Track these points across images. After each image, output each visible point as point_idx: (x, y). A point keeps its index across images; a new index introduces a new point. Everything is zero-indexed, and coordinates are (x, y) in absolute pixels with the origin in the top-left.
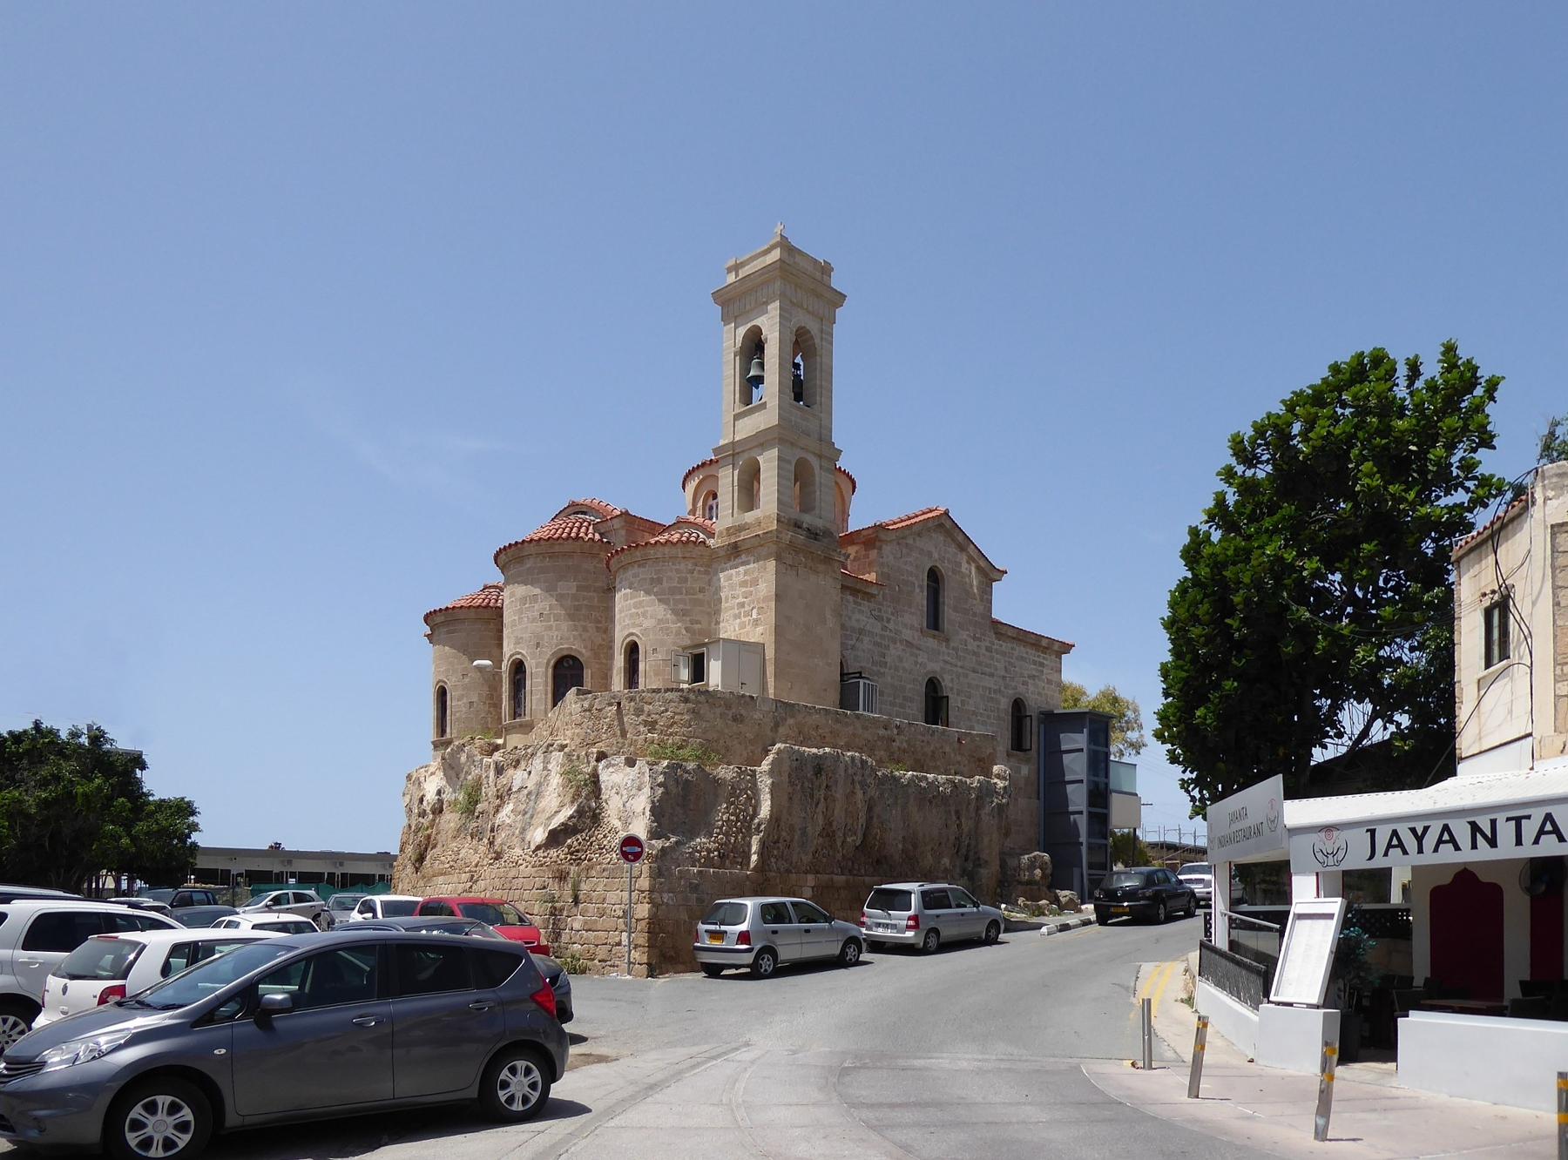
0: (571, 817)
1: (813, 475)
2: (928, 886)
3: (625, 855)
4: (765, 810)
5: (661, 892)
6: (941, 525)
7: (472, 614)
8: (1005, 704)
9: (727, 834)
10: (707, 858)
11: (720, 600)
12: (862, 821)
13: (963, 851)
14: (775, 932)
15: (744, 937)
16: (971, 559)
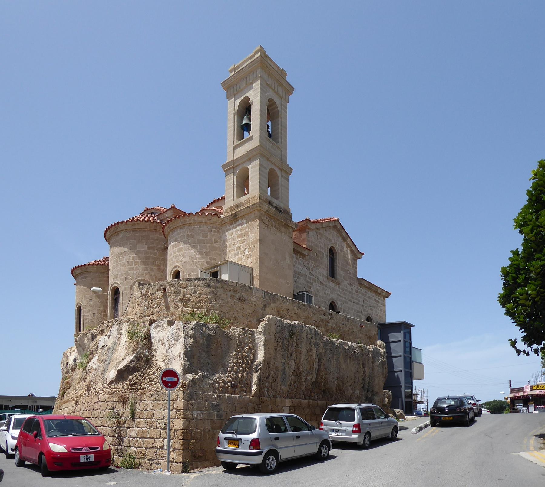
0: (132, 361)
1: (278, 181)
2: (363, 406)
3: (165, 383)
4: (261, 356)
5: (192, 411)
6: (335, 227)
7: (95, 268)
9: (236, 372)
10: (224, 387)
11: (226, 247)
12: (316, 367)
13: (366, 387)
14: (277, 439)
15: (255, 443)
16: (348, 246)
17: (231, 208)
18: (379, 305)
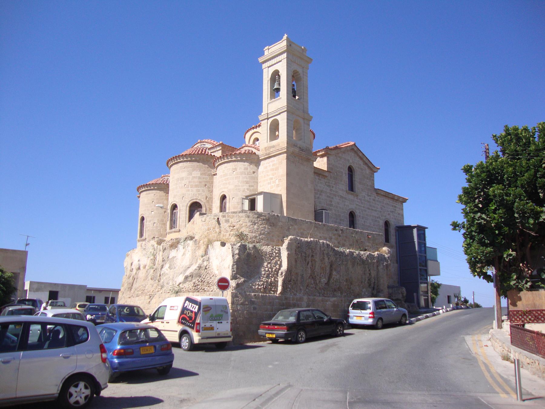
6: (353, 149)
8: (382, 223)
13: (372, 285)
17: (265, 148)
18: (397, 209)
